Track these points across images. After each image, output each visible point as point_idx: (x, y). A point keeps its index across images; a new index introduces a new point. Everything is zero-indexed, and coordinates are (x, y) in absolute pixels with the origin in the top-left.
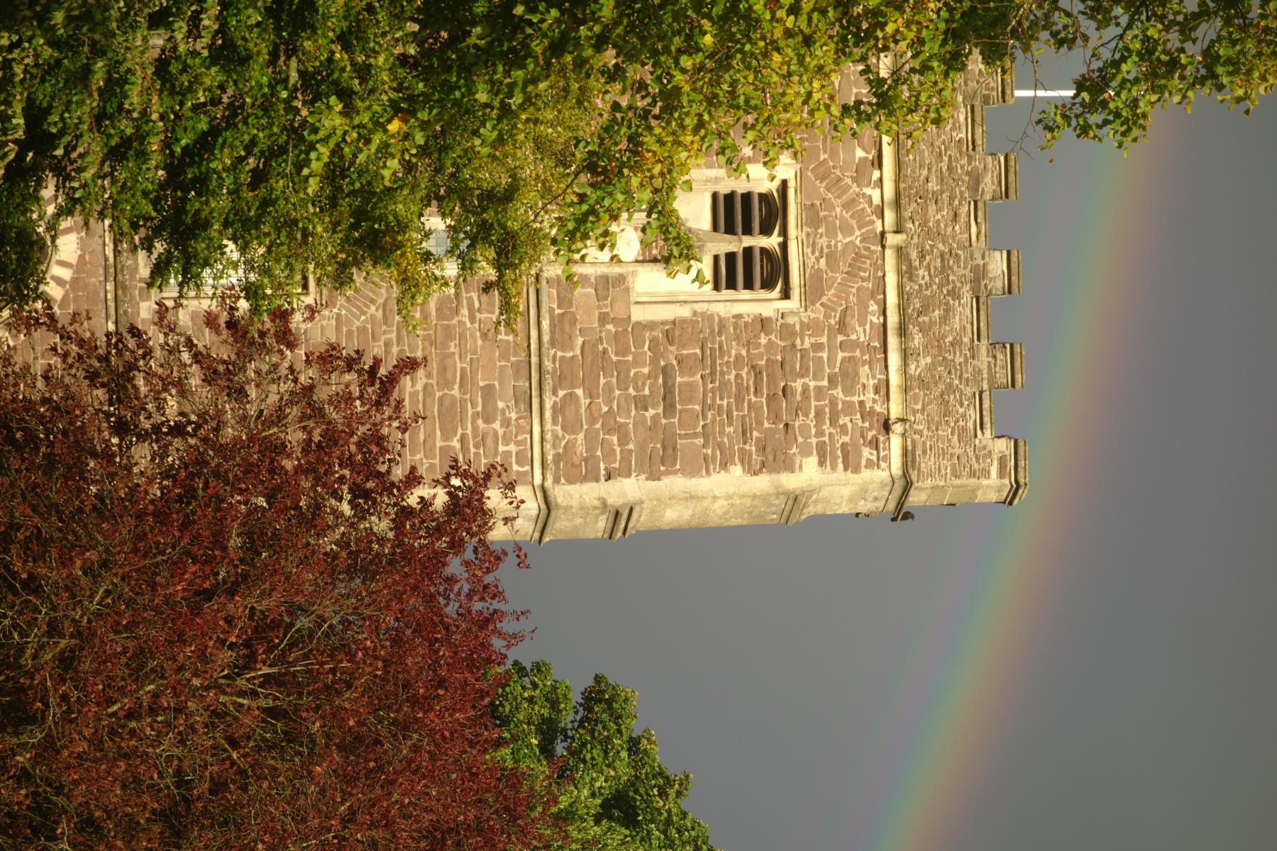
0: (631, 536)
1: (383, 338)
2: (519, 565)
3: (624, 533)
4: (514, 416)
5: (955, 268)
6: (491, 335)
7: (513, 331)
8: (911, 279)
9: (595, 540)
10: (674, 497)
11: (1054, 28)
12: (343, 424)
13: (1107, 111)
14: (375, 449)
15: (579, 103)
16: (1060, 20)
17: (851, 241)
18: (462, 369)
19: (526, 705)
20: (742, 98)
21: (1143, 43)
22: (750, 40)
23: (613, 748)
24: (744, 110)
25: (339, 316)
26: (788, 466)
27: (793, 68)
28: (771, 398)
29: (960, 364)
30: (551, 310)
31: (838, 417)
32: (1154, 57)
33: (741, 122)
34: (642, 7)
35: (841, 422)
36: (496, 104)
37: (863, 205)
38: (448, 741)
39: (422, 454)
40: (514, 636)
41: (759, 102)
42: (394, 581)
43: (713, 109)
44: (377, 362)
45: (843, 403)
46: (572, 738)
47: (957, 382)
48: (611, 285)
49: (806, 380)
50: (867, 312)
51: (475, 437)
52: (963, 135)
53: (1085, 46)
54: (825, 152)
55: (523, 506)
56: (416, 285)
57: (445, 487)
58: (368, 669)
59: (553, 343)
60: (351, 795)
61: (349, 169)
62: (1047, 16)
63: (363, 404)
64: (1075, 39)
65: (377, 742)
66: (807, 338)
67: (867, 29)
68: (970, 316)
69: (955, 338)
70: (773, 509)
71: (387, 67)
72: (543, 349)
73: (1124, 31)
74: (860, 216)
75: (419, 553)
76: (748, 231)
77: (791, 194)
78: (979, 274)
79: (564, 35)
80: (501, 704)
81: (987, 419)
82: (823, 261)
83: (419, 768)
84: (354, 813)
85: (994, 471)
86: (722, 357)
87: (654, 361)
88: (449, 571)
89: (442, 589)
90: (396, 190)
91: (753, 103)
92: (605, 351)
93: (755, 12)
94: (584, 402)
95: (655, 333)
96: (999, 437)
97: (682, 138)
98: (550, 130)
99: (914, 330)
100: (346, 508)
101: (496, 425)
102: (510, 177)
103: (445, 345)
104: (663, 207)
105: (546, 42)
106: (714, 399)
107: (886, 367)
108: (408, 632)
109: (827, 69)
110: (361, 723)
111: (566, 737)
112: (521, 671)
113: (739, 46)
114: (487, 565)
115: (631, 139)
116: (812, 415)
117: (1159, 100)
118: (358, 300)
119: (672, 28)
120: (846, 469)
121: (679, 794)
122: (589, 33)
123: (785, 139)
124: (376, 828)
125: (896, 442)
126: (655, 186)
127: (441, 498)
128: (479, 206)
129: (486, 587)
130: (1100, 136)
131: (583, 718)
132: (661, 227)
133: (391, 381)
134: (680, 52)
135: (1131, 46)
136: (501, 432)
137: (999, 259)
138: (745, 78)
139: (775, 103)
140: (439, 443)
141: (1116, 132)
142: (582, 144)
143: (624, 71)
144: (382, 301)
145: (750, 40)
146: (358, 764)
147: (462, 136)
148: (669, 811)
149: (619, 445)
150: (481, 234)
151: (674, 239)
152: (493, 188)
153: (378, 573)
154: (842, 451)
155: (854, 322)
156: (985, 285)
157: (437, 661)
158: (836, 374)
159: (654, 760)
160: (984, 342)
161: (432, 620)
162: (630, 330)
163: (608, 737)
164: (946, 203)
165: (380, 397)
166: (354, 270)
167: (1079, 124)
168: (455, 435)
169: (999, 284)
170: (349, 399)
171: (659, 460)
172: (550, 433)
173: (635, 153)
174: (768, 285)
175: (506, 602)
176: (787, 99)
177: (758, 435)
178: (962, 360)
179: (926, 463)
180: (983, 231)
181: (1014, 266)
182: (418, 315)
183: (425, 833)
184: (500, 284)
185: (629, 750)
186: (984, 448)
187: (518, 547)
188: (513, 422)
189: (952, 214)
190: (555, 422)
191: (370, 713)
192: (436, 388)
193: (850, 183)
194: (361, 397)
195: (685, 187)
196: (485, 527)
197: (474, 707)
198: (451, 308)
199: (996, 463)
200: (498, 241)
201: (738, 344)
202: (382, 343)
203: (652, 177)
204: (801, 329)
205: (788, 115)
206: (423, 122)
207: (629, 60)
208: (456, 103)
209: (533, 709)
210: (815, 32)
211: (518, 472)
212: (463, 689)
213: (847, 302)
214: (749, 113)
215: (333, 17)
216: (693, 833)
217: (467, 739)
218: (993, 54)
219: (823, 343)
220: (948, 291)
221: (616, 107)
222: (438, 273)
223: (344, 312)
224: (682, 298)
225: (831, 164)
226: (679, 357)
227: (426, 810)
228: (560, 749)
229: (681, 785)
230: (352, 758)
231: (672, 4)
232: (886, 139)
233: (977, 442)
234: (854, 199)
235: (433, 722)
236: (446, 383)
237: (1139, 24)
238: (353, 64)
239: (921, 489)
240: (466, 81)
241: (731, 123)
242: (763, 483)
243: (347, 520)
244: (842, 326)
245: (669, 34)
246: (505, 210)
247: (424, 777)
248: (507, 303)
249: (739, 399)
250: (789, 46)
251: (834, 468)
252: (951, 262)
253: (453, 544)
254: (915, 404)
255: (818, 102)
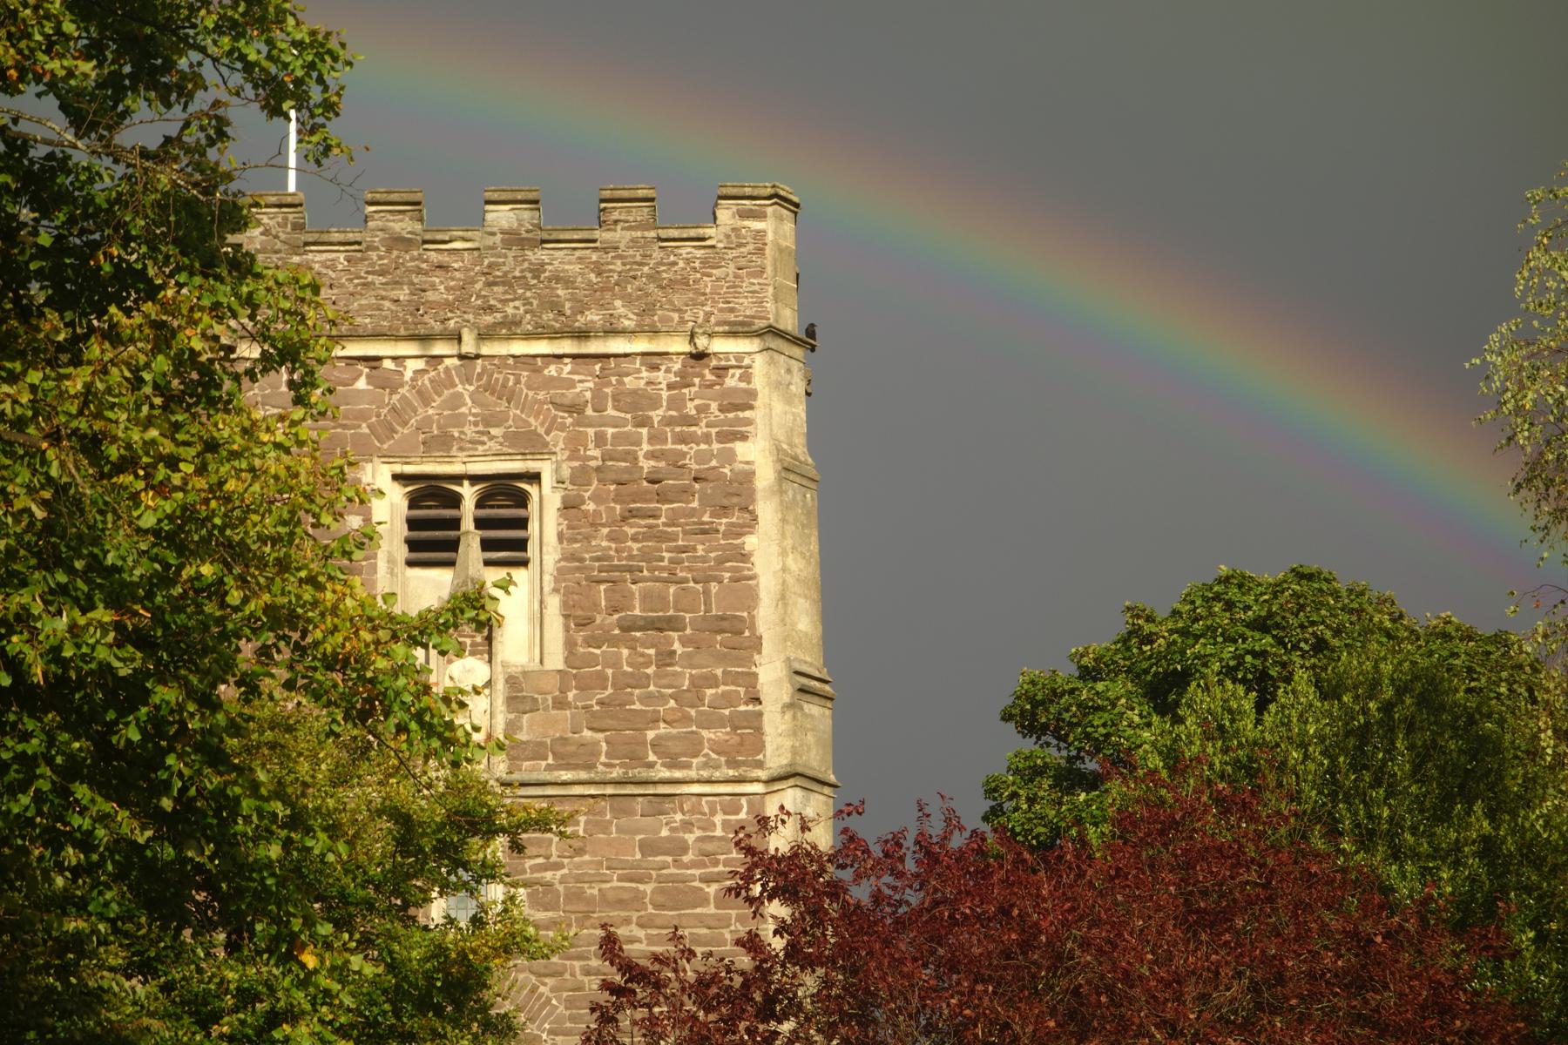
0: (829, 673)
1: (580, 978)
2: (860, 814)
3: (826, 682)
4: (679, 817)
5: (505, 268)
6: (576, 843)
7: (571, 816)
8: (518, 324)
9: (834, 717)
10: (783, 620)
11: (203, 142)
12: (682, 1029)
13: (307, 79)
14: (714, 990)
15: (290, 729)
16: (193, 136)
17: (471, 397)
18: (620, 880)
19: (1038, 807)
20: (280, 529)
21: (224, 33)
22: (209, 519)
23: (1092, 700)
24: (295, 527)
25: (551, 1032)
26: (746, 478)
27: (244, 465)
28: (662, 498)
29: (624, 264)
30: (549, 768)
31: (687, 416)
32: (241, 20)
33: (310, 531)
34: (166, 651)
35: (693, 412)
36: (283, 833)
37: (425, 380)
38: (1076, 905)
39: (724, 931)
40: (948, 820)
41: (286, 508)
42: (877, 968)
43: (295, 564)
44: (607, 986)
45: (669, 409)
46: (1079, 750)
47: (646, 269)
48: (520, 693)
49: (641, 454)
50: (559, 379)
51: (705, 866)
52: (342, 257)
53: (226, 105)
54: (359, 426)
55: (788, 807)
56: (513, 935)
57: (763, 903)
58: (986, 1000)
59: (589, 767)
60: (1141, 1025)
61: (366, 1017)
62: (188, 151)
63: (658, 1004)
64: (217, 117)
65: (1076, 992)
66: (588, 453)
67: (199, 373)
68: (565, 252)
69: (592, 271)
70: (799, 497)
71: (240, 968)
72: (597, 779)
73: (209, 56)
74: (438, 385)
75: (843, 937)
76: (455, 524)
77: (409, 469)
78: (513, 239)
79: (198, 748)
80: (1037, 837)
81: (693, 233)
82: (494, 431)
83: (1109, 942)
84: (1165, 1022)
85: (757, 225)
86: (610, 558)
87: (614, 642)
88: (866, 900)
89: (888, 910)
90: (393, 959)
91: (286, 516)
92: (601, 703)
93: (174, 511)
94: (663, 729)
95: (580, 640)
96: (715, 218)
97: (329, 605)
98: (323, 767)
99: (580, 322)
100: (787, 1027)
101: (690, 838)
102: (380, 817)
103: (590, 901)
104: (415, 629)
105: (207, 771)
106: (662, 569)
107: (626, 355)
108: (941, 952)
109: (247, 424)
110: (1053, 1012)
111: (1078, 757)
112: (995, 812)
113: (216, 532)
114: (859, 853)
115: (329, 668)
116: (684, 448)
117: (294, 15)
118: (532, 1007)
119: (193, 613)
120: (751, 408)
121: (1150, 619)
122: (197, 717)
123: (332, 477)
124: (1182, 995)
125: (719, 346)
126: (389, 638)
127: (777, 909)
128: (416, 856)
129: (887, 855)
130: (337, 88)
131: (1055, 737)
132: (440, 632)
133: (629, 969)
134: (223, 605)
135: (227, 48)
136: (698, 833)
137: (495, 214)
138: (255, 525)
139: (286, 488)
140: (711, 909)
141: (333, 68)
142: (335, 728)
143: (244, 674)
144: (533, 978)
145: (209, 519)
146: (1103, 1017)
147: (329, 876)
148: (1171, 632)
149: (717, 687)
150: (452, 854)
151: (455, 616)
152: (394, 838)
153: (867, 988)
154: (729, 411)
155: (570, 394)
156: (527, 232)
157: (978, 918)
158: (633, 418)
159: (1108, 650)
160: (597, 234)
161: (926, 922)
162: (574, 671)
163: (1079, 706)
164: (424, 278)
165: (649, 983)
166: (493, 1012)
167: (323, 114)
168: (701, 889)
169: (526, 215)
170: (653, 1021)
171: (736, 638)
172: (701, 772)
173: (346, 663)
174: (522, 500)
175: (905, 829)
176: (283, 473)
177: (708, 514)
178: (619, 262)
179: (746, 308)
180: (460, 233)
181: (504, 196)
182: (551, 934)
183: (1189, 935)
184: (512, 832)
185: (1095, 680)
186: (728, 236)
187: (838, 814)
188: (687, 818)
189: (438, 272)
190: (688, 766)
191: (1041, 1000)
192: (643, 913)
193: (398, 396)
194: (649, 1006)
195: (391, 601)
196: (813, 855)
197: (1035, 872)
198: (543, 893)
199: (747, 223)
200: (460, 833)
201: (595, 538)
202: (586, 979)
203: (377, 643)
204: (577, 459)
205: (302, 471)
206: (303, 924)
207: (231, 668)
208: (281, 883)
209: (1043, 798)
210: (201, 438)
211: (748, 813)
212: (1013, 884)
213: (545, 403)
214: (299, 521)
215: (176, 1035)
216: (1198, 602)
217: (1075, 881)
218: (235, 218)
219: (596, 433)
220: (533, 278)
221: (289, 685)
222: (500, 908)
223: (547, 1026)
224: (537, 606)
225: (374, 419)
226: (610, 611)
227: (1161, 933)
228: (1091, 765)
229: (1138, 617)
230: (1095, 1023)
231: (163, 613)
232: (338, 352)
233: (720, 245)
234: (418, 392)
235: (1052, 923)
236: (637, 900)
237: (200, 37)
238: (236, 1010)
239: (777, 315)
240: (254, 871)
241: (312, 542)
242: (766, 511)
243: (802, 1026)
244: (575, 408)
245: (200, 617)
246: (421, 824)
247: (1119, 935)
248: (537, 823)
249: (663, 537)
250: (217, 471)
251: (749, 422)
252: (498, 273)
253: (833, 894)
254: (673, 320)
255: (287, 435)
